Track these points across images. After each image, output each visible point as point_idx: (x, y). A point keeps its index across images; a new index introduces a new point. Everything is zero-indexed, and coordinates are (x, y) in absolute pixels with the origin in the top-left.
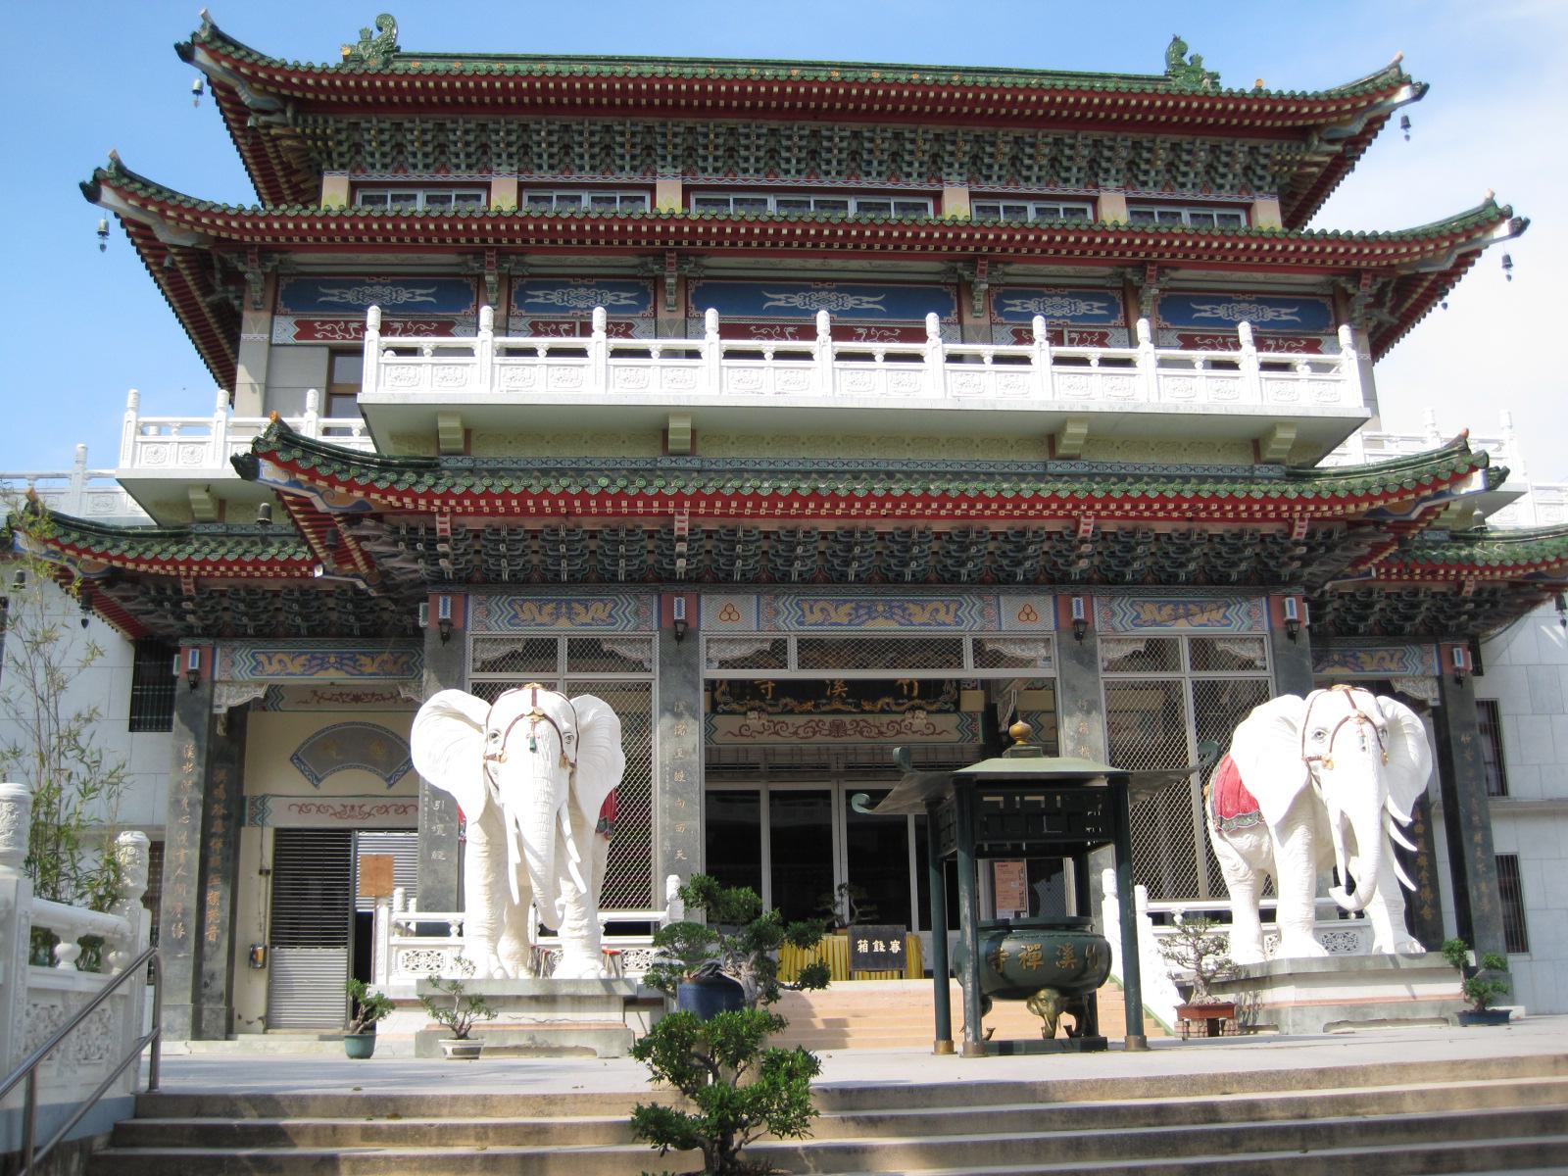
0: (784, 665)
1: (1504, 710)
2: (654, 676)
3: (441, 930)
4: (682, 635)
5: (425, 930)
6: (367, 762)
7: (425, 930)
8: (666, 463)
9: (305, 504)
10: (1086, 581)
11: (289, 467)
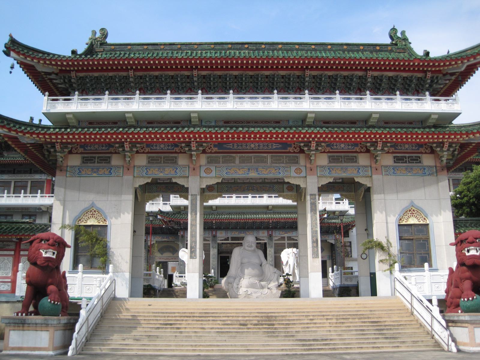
0: (228, 240)
1: (352, 243)
2: (210, 242)
3: (182, 277)
4: (215, 237)
5: (180, 277)
6: (170, 251)
7: (180, 277)
8: (212, 212)
9: (163, 220)
10: (272, 228)
11: (161, 216)
